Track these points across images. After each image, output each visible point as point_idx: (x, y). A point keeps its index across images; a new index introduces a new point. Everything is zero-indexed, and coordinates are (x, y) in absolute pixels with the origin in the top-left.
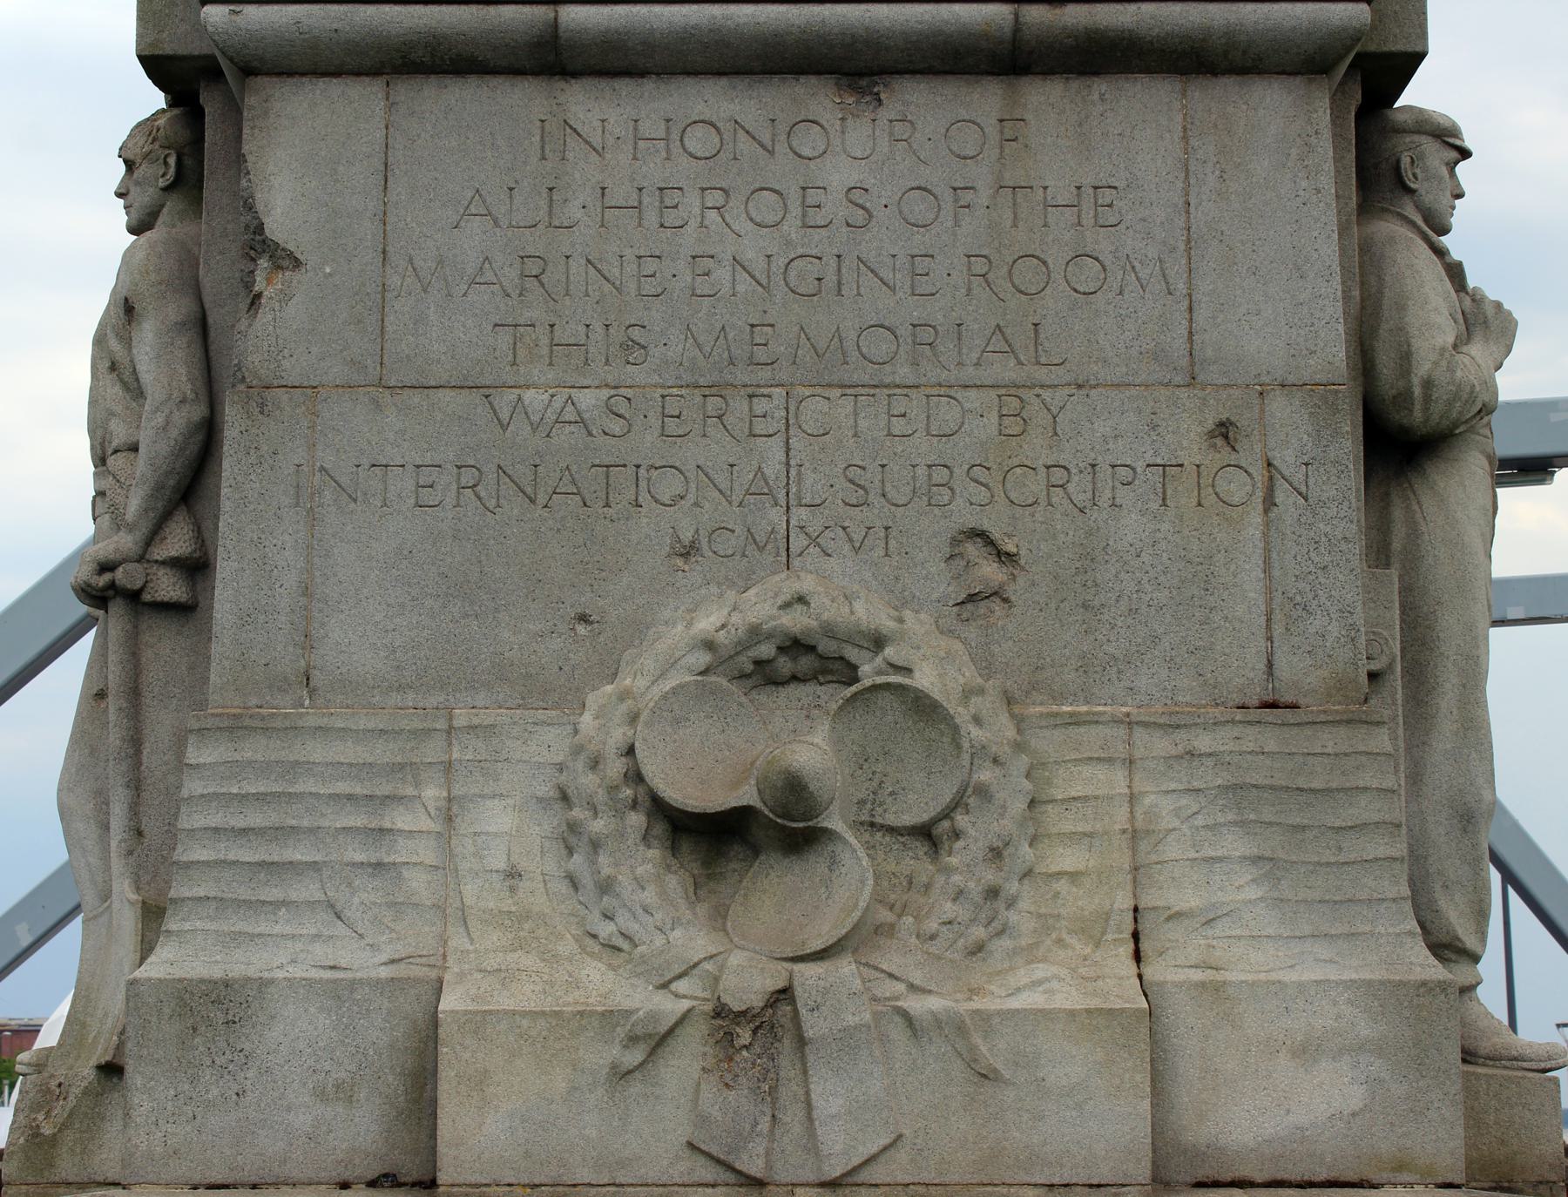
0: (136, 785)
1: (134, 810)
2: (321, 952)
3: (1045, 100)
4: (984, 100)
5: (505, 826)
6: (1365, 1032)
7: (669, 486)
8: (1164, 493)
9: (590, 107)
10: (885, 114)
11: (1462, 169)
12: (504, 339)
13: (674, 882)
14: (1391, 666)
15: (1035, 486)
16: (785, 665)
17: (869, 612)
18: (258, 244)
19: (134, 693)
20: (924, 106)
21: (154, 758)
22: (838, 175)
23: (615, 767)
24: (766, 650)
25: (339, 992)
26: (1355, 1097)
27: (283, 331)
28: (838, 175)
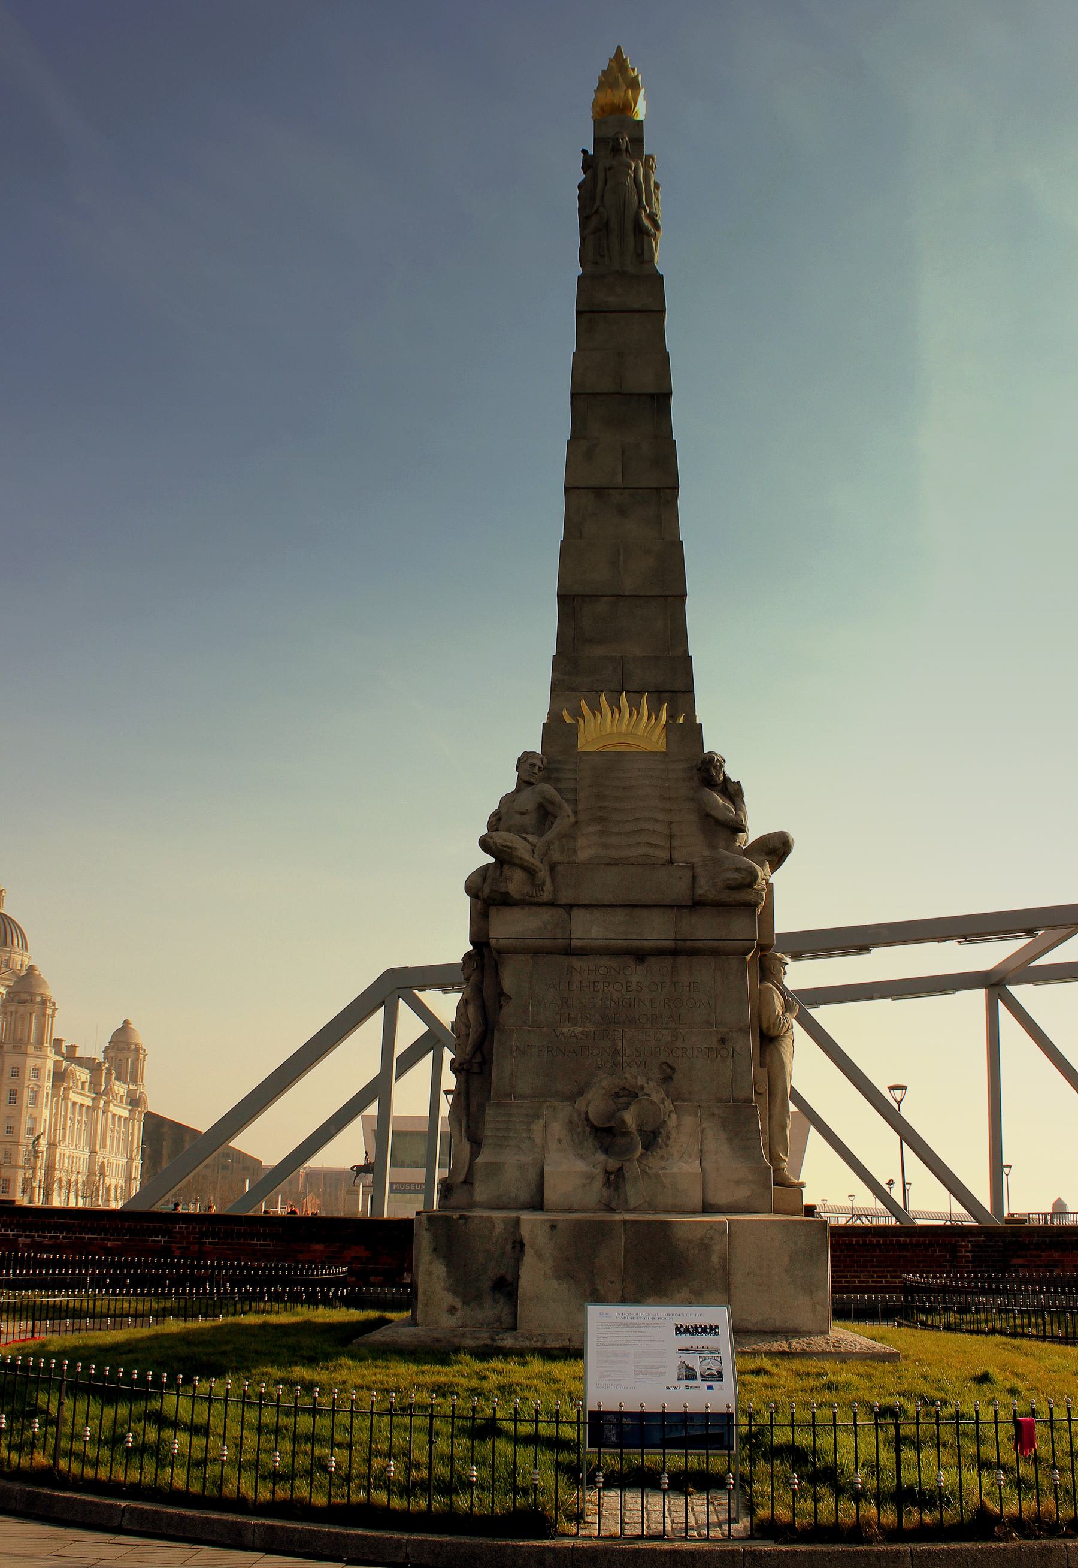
0: (468, 1115)
1: (468, 1122)
2: (516, 1157)
3: (682, 960)
4: (668, 961)
5: (557, 1128)
6: (750, 1178)
7: (595, 1052)
8: (494, 1455)
9: (577, 963)
10: (645, 965)
11: (786, 967)
12: (558, 1016)
13: (72, 1156)
14: (298, 1314)
15: (679, 1052)
16: (621, 1093)
17: (641, 1081)
18: (501, 994)
19: (467, 1093)
20: (653, 962)
21: (473, 1109)
22: (634, 979)
23: (583, 1116)
24: (617, 1090)
25: (521, 1167)
26: (749, 1193)
27: (508, 1015)
28: (634, 979)
